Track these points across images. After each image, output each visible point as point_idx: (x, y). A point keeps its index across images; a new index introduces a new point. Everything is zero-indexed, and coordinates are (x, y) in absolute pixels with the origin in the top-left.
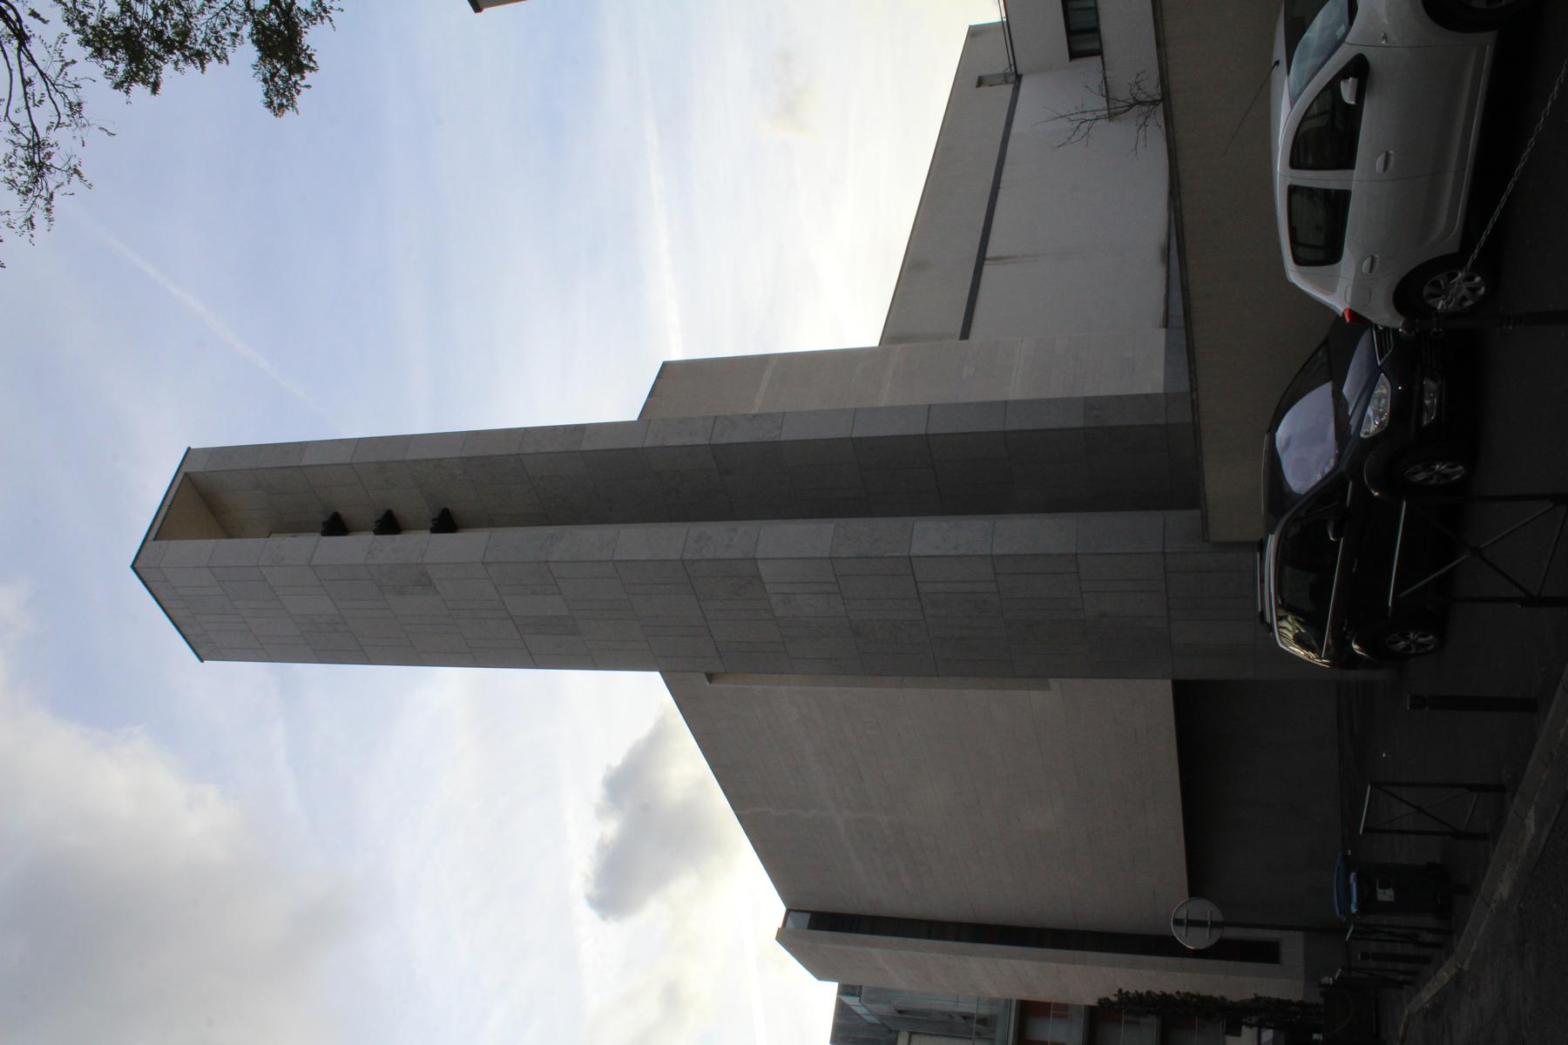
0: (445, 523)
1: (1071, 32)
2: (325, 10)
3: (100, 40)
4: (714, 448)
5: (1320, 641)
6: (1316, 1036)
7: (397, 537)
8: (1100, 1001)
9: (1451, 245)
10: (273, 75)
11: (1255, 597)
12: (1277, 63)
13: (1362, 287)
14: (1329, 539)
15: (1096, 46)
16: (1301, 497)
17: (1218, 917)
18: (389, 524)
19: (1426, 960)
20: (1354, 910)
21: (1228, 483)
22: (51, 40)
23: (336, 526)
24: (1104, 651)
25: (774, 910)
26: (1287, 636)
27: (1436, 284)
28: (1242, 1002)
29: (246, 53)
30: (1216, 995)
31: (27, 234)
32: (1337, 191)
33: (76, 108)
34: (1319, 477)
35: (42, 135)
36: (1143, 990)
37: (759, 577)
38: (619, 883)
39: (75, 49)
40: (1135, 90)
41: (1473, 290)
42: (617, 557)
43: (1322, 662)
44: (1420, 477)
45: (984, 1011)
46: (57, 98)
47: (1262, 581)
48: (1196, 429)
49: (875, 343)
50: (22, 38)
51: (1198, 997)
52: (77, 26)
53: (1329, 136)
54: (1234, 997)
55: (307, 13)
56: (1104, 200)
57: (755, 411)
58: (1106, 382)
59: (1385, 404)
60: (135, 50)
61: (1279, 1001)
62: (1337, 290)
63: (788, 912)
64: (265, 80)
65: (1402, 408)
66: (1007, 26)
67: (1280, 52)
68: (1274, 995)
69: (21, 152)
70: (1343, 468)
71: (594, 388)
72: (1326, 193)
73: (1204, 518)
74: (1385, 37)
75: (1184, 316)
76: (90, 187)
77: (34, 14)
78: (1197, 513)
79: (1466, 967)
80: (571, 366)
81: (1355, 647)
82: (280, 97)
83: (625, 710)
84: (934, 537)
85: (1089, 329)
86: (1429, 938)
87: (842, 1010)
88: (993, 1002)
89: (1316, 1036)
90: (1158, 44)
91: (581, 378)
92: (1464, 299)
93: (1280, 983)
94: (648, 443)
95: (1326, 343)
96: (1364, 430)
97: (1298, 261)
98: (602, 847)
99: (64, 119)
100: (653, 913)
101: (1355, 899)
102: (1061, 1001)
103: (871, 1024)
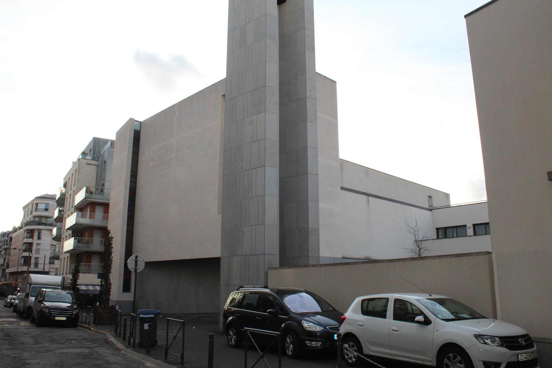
5: (233, 306)
6: (98, 303)
13: (353, 322)
15: (440, 237)
16: (283, 301)
17: (138, 271)
19: (124, 339)
21: (287, 277)
24: (231, 232)
26: (236, 295)
27: (353, 346)
30: (112, 270)
32: (386, 315)
34: (289, 307)
36: (113, 245)
37: (259, 113)
38: (147, 60)
41: (351, 358)
43: (226, 307)
44: (288, 340)
45: (105, 191)
51: (111, 264)
53: (404, 312)
54: (111, 276)
56: (385, 237)
62: (353, 314)
63: (141, 122)
65: (312, 335)
70: (292, 314)
73: (276, 268)
75: (346, 263)
78: (278, 266)
79: (122, 352)
81: (231, 318)
83: (210, 67)
84: (272, 175)
85: (343, 230)
86: (132, 340)
87: (105, 141)
88: (109, 194)
89: (98, 303)
90: (439, 256)
92: (348, 355)
94: (308, 75)
95: (335, 310)
97: (363, 301)
101: (145, 316)
102: (109, 218)
103: (101, 151)
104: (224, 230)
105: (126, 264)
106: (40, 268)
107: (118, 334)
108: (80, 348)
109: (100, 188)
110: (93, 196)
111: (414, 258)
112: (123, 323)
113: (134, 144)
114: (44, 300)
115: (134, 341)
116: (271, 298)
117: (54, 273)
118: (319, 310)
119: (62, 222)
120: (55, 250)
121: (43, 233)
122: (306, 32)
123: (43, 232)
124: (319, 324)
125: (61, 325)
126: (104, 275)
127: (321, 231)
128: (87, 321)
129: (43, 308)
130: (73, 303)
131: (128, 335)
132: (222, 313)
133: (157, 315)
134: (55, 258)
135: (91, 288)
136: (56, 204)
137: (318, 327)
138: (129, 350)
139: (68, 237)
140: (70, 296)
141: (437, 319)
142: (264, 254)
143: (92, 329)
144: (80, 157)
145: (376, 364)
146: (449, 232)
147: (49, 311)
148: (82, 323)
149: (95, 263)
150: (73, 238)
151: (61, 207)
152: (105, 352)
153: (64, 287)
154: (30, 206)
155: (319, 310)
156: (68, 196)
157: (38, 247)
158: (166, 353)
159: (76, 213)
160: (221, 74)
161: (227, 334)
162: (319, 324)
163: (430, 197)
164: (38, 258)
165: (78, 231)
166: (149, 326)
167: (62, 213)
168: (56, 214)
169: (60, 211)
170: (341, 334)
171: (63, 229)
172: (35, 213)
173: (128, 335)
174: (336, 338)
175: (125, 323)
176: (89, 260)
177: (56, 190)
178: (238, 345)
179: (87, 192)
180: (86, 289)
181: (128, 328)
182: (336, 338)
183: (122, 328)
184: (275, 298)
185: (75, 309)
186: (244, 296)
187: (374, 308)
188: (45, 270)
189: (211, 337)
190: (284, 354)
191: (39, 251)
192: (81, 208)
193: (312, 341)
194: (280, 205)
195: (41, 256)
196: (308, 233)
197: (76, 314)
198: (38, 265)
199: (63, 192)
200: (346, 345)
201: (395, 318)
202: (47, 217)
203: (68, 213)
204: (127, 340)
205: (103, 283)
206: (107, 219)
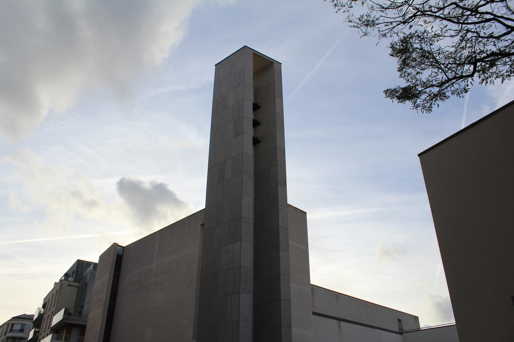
0: (256, 141)
2: (417, 107)
3: (405, 41)
4: (278, 228)
7: (252, 126)
18: (256, 124)
22: (404, 31)
23: (256, 107)
25: (124, 243)
29: (403, 83)
31: (346, 20)
33: (385, 35)
35: (376, 26)
38: (129, 189)
39: (401, 36)
42: (243, 195)
45: (84, 312)
46: (387, 31)
49: (311, 283)
50: (404, 23)
55: (416, 102)
57: (290, 242)
64: (395, 89)
66: (419, 330)
69: (371, 19)
71: (298, 190)
76: (361, 37)
82: (390, 93)
83: (191, 196)
84: (246, 300)
87: (89, 264)
88: (87, 316)
91: (302, 185)
98: (140, 182)
99: (381, 33)
100: (119, 200)
103: (83, 273)
136: (32, 324)
144: (63, 279)
151: (37, 328)
154: (6, 326)
156: (45, 316)
163: (399, 320)
172: (8, 335)
179: (65, 313)
199: (42, 312)
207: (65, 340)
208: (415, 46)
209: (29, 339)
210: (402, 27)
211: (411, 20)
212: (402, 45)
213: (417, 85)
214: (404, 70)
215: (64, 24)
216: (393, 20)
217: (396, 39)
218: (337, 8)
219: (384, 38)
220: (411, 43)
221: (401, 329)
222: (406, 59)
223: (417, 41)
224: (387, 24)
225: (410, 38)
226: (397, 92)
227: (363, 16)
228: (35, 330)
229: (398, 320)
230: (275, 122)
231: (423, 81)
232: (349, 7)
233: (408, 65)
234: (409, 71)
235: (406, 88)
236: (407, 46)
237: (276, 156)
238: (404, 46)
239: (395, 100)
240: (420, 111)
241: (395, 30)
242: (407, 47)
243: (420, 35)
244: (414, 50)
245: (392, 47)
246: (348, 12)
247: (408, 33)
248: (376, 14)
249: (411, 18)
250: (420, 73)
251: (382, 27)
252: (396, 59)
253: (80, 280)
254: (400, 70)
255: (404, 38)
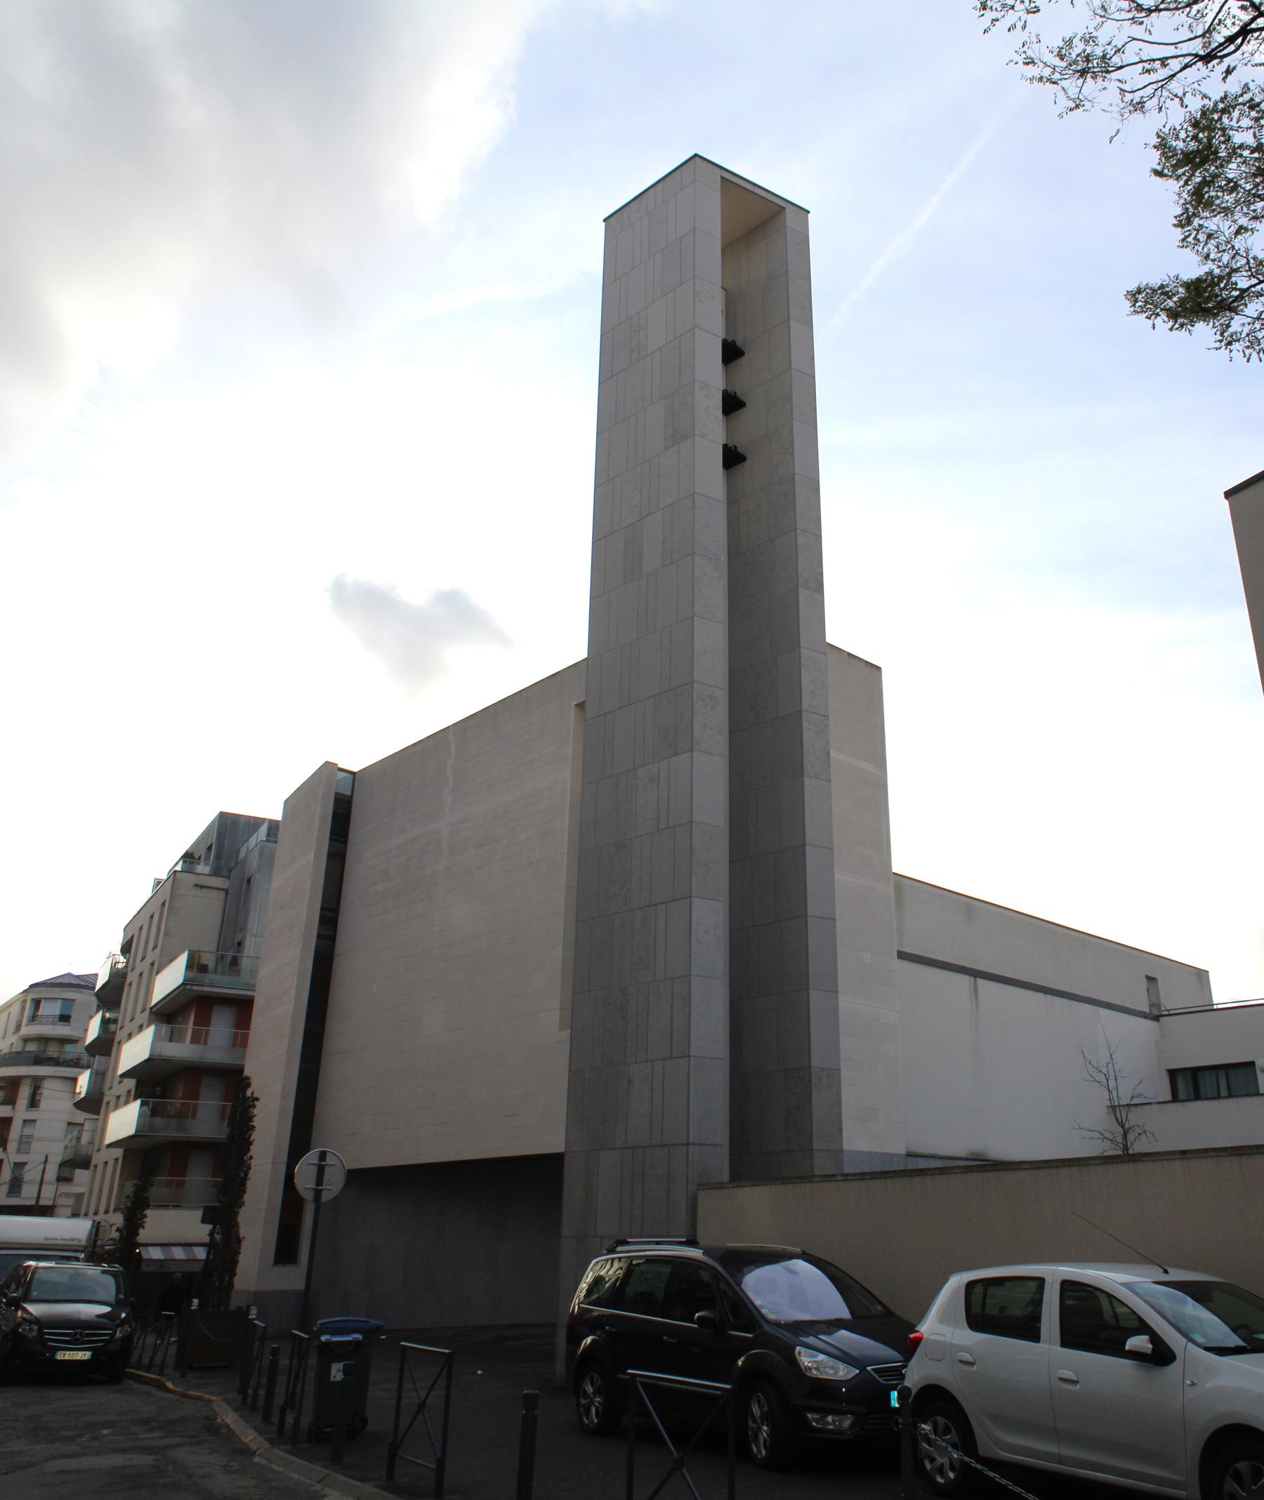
0: (732, 458)
1: (1195, 1072)
2: (1230, 343)
3: (1205, 123)
5: (597, 1303)
6: (196, 1302)
8: (247, 1078)
9: (986, 1447)
10: (1166, 294)
11: (641, 1236)
12: (1166, 1272)
13: (945, 1351)
14: (697, 1305)
15: (1182, 1095)
16: (739, 1285)
17: (325, 1197)
18: (732, 404)
19: (266, 1418)
20: (323, 1338)
21: (752, 1212)
22: (1205, 88)
23: (731, 353)
24: (597, 1080)
26: (605, 1268)
27: (947, 1431)
28: (237, 1224)
29: (1191, 267)
30: (246, 1197)
32: (1038, 1330)
33: (1139, 106)
34: (758, 1303)
35: (1114, 75)
36: (256, 1122)
37: (676, 753)
38: (366, 603)
39: (1195, 105)
40: (1138, 1130)
41: (941, 1470)
43: (575, 1305)
44: (756, 1410)
45: (245, 963)
46: (1149, 90)
47: (658, 1243)
48: (808, 1178)
50: (1207, 58)
51: (245, 1178)
52: (1221, 106)
53: (1095, 1323)
54: (244, 1215)
55: (1228, 326)
56: (1028, 1096)
57: (832, 754)
58: (856, 1092)
59: (828, 1374)
60: (1196, 159)
61: (235, 1262)
62: (942, 1325)
63: (353, 773)
64: (1162, 287)
65: (823, 1391)
66: (1209, 1009)
67: (1176, 1275)
68: (242, 1258)
69: (1099, 52)
70: (767, 1328)
72: (1037, 1318)
73: (721, 1186)
74: (1193, 1384)
75: (917, 1170)
77: (1229, 71)
78: (726, 1178)
79: (257, 1459)
80: (879, 577)
81: (589, 1339)
82: (1147, 300)
83: (541, 624)
84: (709, 921)
85: (903, 1078)
86: (290, 1420)
87: (253, 824)
88: (254, 972)
89: (196, 1302)
90: (1183, 1152)
92: (932, 1460)
93: (254, 1268)
94: (804, 653)
95: (888, 1313)
96: (803, 1350)
97: (970, 1286)
99: (1128, 97)
101: (335, 1339)
102: (251, 1040)
103: (238, 851)
104: (574, 1073)
105: (290, 1177)
106: (28, 1195)
107: (249, 1400)
108: (124, 1450)
109: (231, 954)
110: (208, 978)
111: (1110, 1157)
112: (266, 1363)
113: (332, 833)
114: (27, 1298)
115: (297, 1420)
116: (705, 1276)
117: (69, 1211)
118: (843, 1312)
119: (109, 1055)
120: (79, 1139)
121: (48, 1089)
122: (800, 539)
123: (47, 1084)
124: (845, 1357)
125: (74, 1376)
126: (222, 1215)
127: (846, 1076)
128: (158, 1360)
129: (20, 1324)
130: (117, 1305)
131: (279, 1400)
132: (563, 1321)
133: (371, 1333)
134: (76, 1162)
135: (179, 1253)
136: (94, 1001)
137: (841, 1366)
138: (278, 1452)
139: (123, 1099)
140: (110, 1282)
141: (1190, 1345)
142: (688, 1144)
143: (170, 1385)
144: (178, 868)
145: (1018, 1490)
146: (1207, 1083)
147: (41, 1334)
148: (139, 1367)
149: (199, 1178)
150: (139, 1102)
151: (109, 1010)
152: (202, 1461)
153: (93, 1252)
154: (17, 1007)
155: (845, 1313)
156: (132, 977)
157: (27, 1131)
158: (392, 1458)
159: (152, 1028)
160: (571, 645)
161: (578, 1391)
162: (845, 1357)
163: (1151, 979)
164: (24, 1164)
165: (152, 1081)
166: (346, 1371)
167: (112, 1027)
168: (93, 1030)
169: (105, 1022)
170: (908, 1390)
171: (109, 1074)
172: (26, 1030)
173: (279, 1400)
174: (895, 1403)
175: (274, 1364)
176: (179, 1169)
177: (96, 958)
178: (608, 1429)
179: (190, 966)
180: (162, 1257)
181: (282, 1378)
182: (895, 1403)
183: (264, 1380)
184: (716, 1276)
185: (124, 1321)
186: (630, 1271)
187: (1003, 1309)
188: (42, 1203)
189: (530, 1403)
190: (745, 1454)
191: (29, 1143)
192: (168, 1014)
193: (825, 1412)
194: (732, 1003)
195: (33, 1159)
196: (810, 1081)
197: (122, 1339)
198: (20, 1186)
199: (120, 966)
200: (926, 1427)
201: (1065, 1343)
202: (63, 1041)
203: (129, 1027)
204: (275, 1419)
205: (218, 1237)
206: (244, 1044)
207: (192, 1042)
208: (1238, 138)
209: (88, 1042)
210: (1198, 76)
211: (1232, 48)
212: (1195, 137)
213: (1236, 270)
214: (1196, 222)
215: (111, 80)
216: (1170, 51)
217: (1176, 117)
218: (990, 15)
219: (1138, 116)
220: (1223, 130)
221: (1155, 1004)
222: (1205, 183)
223: (1246, 122)
224: (1148, 66)
225: (1224, 111)
226: (1168, 295)
227: (1071, 40)
228: (103, 1017)
229: (1148, 978)
230: (788, 399)
231: (1255, 258)
232: (1028, 12)
233: (1209, 204)
234: (1213, 223)
235: (1199, 280)
236: (1210, 139)
237: (794, 501)
238: (1200, 141)
239: (1163, 322)
240: (1237, 356)
241: (1174, 86)
242: (1210, 145)
243: (1257, 100)
244: (1234, 152)
245: (1163, 145)
246: (1024, 27)
247: (1216, 96)
248: (1113, 32)
249: (1231, 40)
250: (1246, 230)
251: (1134, 78)
252: (1173, 186)
253: (230, 870)
254: (1184, 221)
255: (1204, 113)
